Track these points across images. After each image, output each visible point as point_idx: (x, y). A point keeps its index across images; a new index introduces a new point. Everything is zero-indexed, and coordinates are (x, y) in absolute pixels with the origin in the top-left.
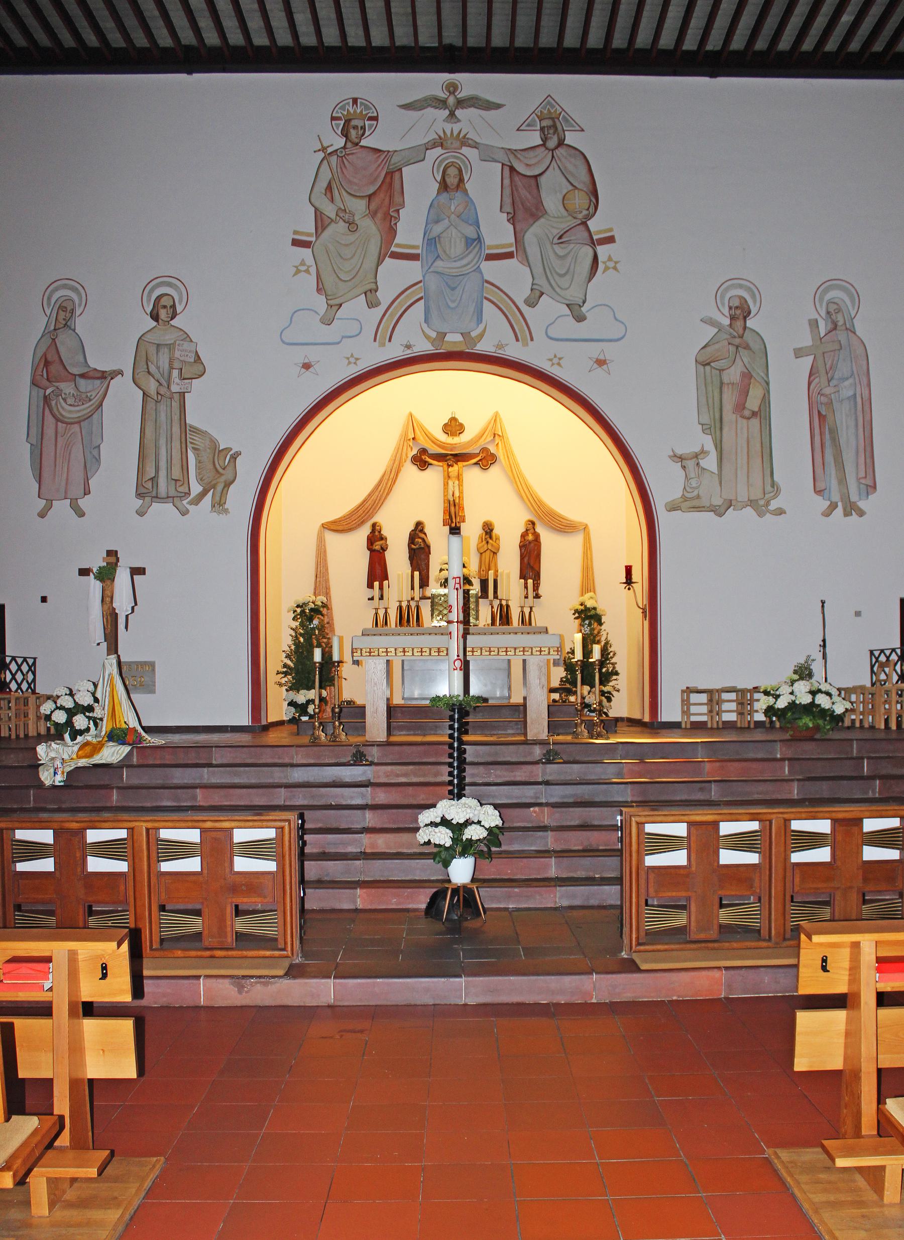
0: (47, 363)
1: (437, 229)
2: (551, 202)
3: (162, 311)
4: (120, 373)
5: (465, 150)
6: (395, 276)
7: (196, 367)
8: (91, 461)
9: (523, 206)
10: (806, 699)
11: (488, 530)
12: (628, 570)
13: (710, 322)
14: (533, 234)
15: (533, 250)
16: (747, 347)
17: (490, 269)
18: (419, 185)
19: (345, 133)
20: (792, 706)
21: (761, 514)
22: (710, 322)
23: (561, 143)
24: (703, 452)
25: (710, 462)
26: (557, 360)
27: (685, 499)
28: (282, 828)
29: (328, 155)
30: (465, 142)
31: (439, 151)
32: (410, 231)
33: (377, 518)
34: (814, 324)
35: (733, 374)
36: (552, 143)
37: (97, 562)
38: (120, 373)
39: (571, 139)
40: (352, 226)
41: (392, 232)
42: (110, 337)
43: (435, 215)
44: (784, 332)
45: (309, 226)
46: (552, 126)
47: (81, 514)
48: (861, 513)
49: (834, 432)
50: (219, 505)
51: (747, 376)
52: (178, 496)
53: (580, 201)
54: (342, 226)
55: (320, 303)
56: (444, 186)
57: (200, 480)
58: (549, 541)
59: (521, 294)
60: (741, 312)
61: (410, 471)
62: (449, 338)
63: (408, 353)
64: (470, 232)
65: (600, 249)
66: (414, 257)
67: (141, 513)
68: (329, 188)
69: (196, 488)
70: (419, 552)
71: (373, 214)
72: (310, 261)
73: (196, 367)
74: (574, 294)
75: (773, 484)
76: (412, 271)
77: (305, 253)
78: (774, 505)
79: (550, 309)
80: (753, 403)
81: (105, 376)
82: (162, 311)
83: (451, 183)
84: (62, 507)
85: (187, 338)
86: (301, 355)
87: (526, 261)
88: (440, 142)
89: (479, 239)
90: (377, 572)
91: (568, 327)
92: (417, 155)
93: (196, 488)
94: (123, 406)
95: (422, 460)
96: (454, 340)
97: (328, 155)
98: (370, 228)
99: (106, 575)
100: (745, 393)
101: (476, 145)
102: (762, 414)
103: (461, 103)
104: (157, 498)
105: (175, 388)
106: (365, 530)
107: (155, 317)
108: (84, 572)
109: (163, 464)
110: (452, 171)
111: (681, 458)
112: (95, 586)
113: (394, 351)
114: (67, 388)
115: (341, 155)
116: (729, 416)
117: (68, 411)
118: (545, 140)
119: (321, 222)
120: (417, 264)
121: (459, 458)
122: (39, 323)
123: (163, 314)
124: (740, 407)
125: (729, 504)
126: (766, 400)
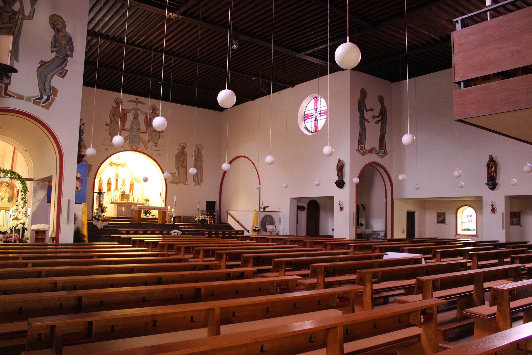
1: (133, 126)
11: (124, 181)
13: (178, 149)
17: (142, 135)
18: (130, 117)
19: (117, 104)
23: (155, 113)
25: (177, 175)
26: (152, 154)
30: (138, 110)
32: (128, 125)
34: (195, 151)
35: (181, 159)
41: (124, 125)
43: (133, 123)
44: (191, 151)
45: (109, 122)
51: (184, 160)
56: (134, 118)
59: (147, 140)
60: (183, 148)
64: (138, 127)
65: (161, 134)
66: (128, 131)
70: (109, 184)
77: (108, 127)
83: (136, 118)
88: (134, 109)
92: (130, 111)
96: (134, 147)
100: (183, 163)
101: (140, 111)
116: (180, 167)
119: (111, 121)
124: (182, 165)
125: (179, 183)
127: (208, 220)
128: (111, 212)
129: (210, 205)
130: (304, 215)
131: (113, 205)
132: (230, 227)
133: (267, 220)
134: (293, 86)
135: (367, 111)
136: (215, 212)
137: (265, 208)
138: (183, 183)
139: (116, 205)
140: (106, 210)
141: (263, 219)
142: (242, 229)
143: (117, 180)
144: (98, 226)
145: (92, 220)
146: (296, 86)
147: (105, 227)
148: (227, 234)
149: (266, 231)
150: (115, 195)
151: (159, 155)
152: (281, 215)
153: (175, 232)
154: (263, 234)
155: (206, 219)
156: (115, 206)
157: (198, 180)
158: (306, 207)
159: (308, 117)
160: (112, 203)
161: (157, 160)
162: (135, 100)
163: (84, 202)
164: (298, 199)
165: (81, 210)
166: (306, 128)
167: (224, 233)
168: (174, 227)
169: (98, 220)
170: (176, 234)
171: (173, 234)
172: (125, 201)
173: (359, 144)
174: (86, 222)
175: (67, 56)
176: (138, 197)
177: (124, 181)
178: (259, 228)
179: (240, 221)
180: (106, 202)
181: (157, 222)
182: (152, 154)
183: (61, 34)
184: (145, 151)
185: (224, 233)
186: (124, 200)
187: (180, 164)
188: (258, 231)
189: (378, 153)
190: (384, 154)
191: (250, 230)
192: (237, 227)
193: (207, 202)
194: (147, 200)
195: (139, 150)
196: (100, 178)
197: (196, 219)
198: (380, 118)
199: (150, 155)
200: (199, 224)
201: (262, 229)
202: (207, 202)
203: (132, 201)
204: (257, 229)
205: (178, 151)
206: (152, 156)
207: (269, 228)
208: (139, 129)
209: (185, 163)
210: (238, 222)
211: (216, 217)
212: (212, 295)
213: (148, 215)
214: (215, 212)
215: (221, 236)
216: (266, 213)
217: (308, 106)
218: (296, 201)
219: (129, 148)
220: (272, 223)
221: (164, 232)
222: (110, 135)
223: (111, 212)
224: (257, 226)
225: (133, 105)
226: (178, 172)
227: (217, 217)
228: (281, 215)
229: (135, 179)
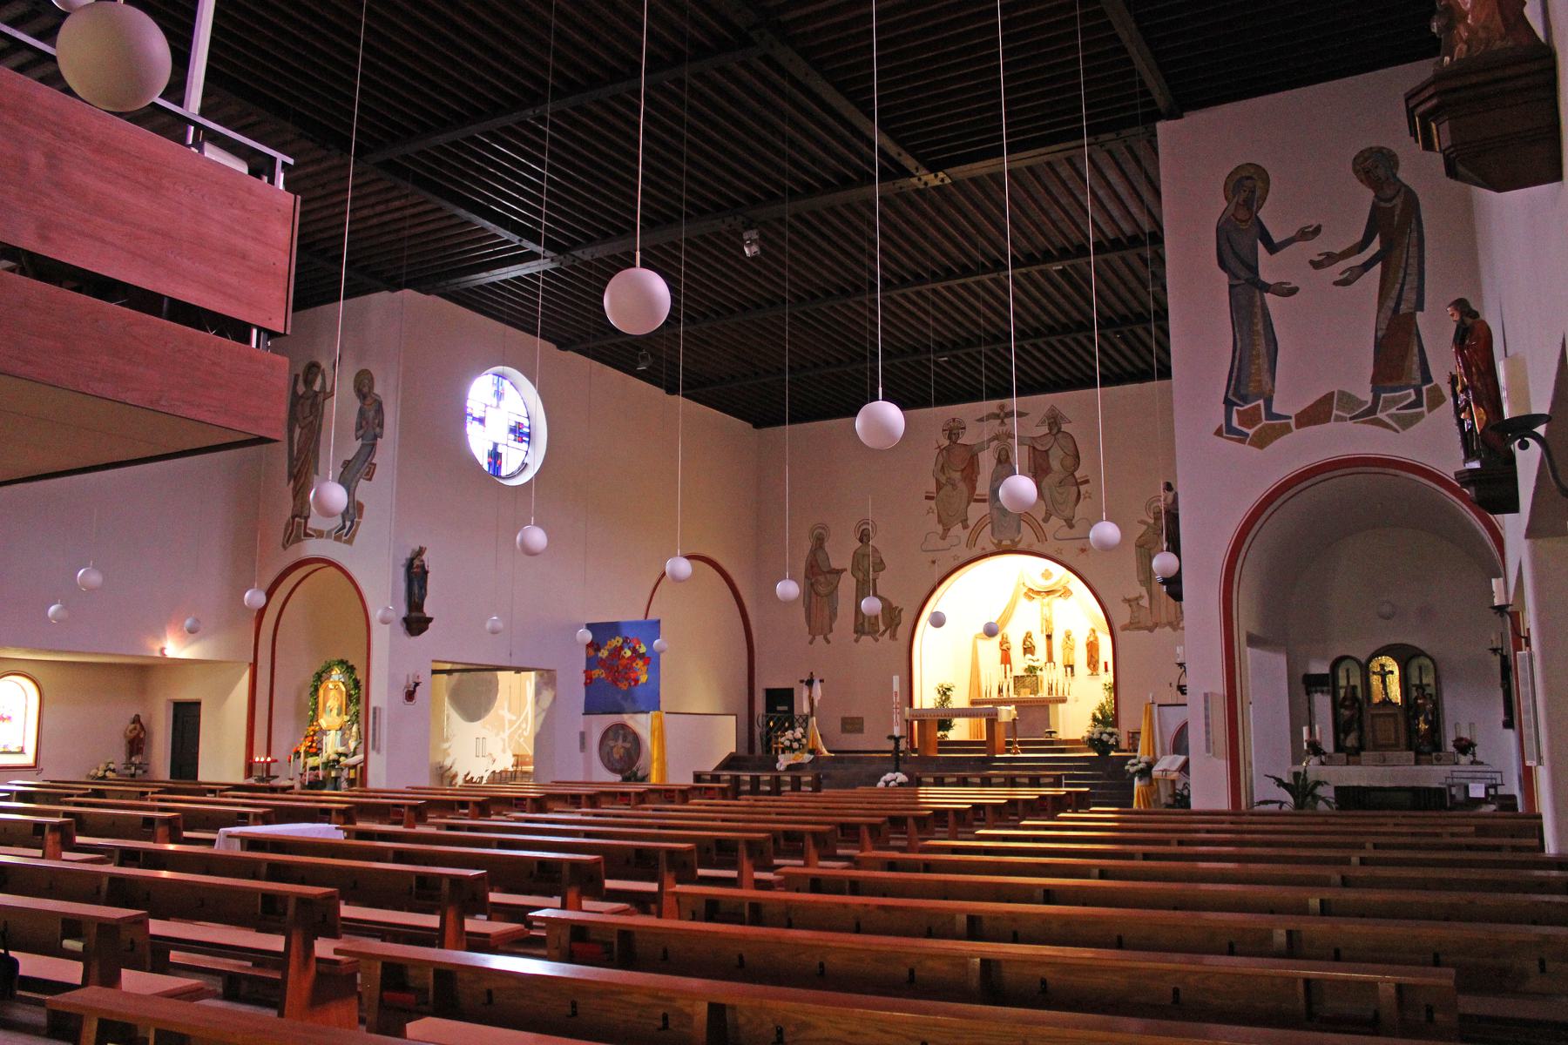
2: (1055, 464)
3: (864, 537)
6: (976, 512)
7: (880, 566)
8: (833, 615)
23: (1059, 431)
24: (1141, 597)
25: (1145, 602)
26: (1060, 551)
28: (22, 752)
39: (1064, 428)
40: (954, 486)
41: (974, 488)
42: (840, 555)
45: (932, 487)
46: (1054, 421)
47: (828, 642)
50: (893, 637)
53: (1069, 461)
54: (949, 487)
55: (940, 528)
56: (999, 461)
61: (1023, 601)
65: (1083, 488)
66: (984, 501)
67: (857, 641)
69: (882, 628)
73: (880, 566)
74: (1068, 513)
76: (984, 508)
77: (932, 503)
79: (1055, 522)
81: (839, 572)
82: (864, 537)
84: (820, 638)
86: (931, 556)
88: (996, 438)
90: (1006, 659)
91: (1065, 532)
93: (882, 628)
95: (1032, 593)
96: (1006, 542)
98: (962, 487)
99: (810, 683)
104: (864, 633)
107: (861, 540)
111: (1128, 601)
113: (977, 551)
114: (821, 579)
115: (947, 449)
117: (822, 589)
119: (939, 486)
121: (1049, 593)
122: (807, 545)
125: (1156, 625)
135: (1272, 248)
138: (1170, 624)
143: (1049, 637)
146: (570, 354)
148: (766, 783)
167: (755, 782)
172: (1026, 694)
173: (1228, 403)
175: (375, 437)
182: (1060, 551)
183: (369, 401)
184: (1037, 547)
185: (755, 782)
189: (1372, 410)
190: (1417, 403)
195: (1021, 546)
198: (1375, 246)
199: (957, 563)
205: (1144, 527)
206: (1060, 557)
212: (665, 957)
215: (747, 788)
221: (1491, 808)
222: (940, 521)
226: (1150, 592)
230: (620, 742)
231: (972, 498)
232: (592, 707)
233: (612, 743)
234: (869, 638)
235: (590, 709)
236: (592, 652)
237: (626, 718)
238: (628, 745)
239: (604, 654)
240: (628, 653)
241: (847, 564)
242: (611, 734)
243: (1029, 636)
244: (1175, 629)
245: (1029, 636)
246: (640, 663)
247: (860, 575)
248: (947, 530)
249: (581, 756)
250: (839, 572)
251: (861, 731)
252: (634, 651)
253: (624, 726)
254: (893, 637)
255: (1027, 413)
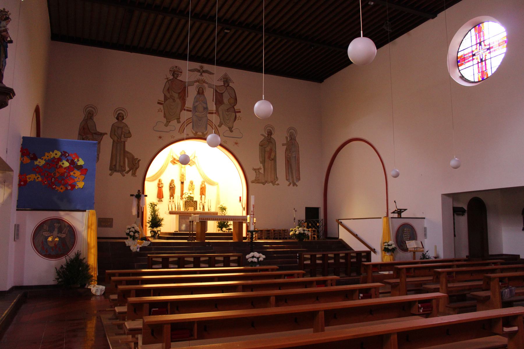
0: (84, 129)
1: (196, 104)
2: (226, 101)
3: (120, 117)
4: (106, 134)
5: (204, 84)
9: (219, 101)
10: (302, 232)
11: (192, 183)
12: (240, 197)
13: (263, 135)
14: (222, 108)
15: (220, 113)
16: (271, 142)
18: (192, 92)
19: (173, 75)
20: (300, 233)
21: (274, 185)
22: (263, 135)
23: (228, 85)
24: (260, 168)
25: (262, 171)
27: (256, 180)
29: (168, 80)
31: (197, 83)
32: (189, 103)
33: (161, 178)
34: (287, 138)
35: (268, 149)
36: (226, 85)
37: (136, 193)
38: (106, 134)
39: (231, 85)
41: (184, 103)
42: (104, 123)
43: (196, 100)
44: (280, 138)
45: (163, 99)
46: (226, 81)
48: (297, 186)
49: (291, 165)
50: (134, 174)
51: (271, 150)
52: (122, 170)
53: (232, 101)
55: (165, 121)
56: (199, 93)
57: (129, 167)
58: (208, 188)
60: (270, 133)
61: (170, 164)
62: (199, 133)
63: (188, 137)
64: (205, 105)
65: (237, 114)
66: (190, 111)
67: (111, 175)
68: (168, 89)
69: (127, 169)
70: (172, 189)
71: (180, 98)
72: (162, 108)
75: (277, 177)
76: (189, 115)
77: (161, 106)
78: (277, 183)
80: (272, 157)
81: (102, 135)
82: (120, 117)
83: (201, 92)
85: (127, 126)
87: (219, 115)
88: (198, 81)
89: (207, 108)
91: (228, 133)
92: (191, 84)
93: (127, 169)
94: (107, 143)
97: (168, 80)
98: (178, 101)
101: (207, 83)
102: (274, 160)
103: (204, 72)
104: (116, 171)
105: (122, 140)
106: (157, 182)
107: (117, 119)
108: (132, 195)
109: (118, 160)
110: (201, 89)
111: (255, 169)
112: (135, 201)
116: (267, 160)
118: (224, 84)
119: (166, 98)
120: (190, 113)
123: (120, 118)
124: (269, 157)
125: (266, 182)
126: (275, 156)
127: (310, 234)
128: (170, 225)
129: (312, 214)
130: (463, 221)
131: (174, 216)
132: (343, 245)
133: (404, 232)
134: (434, 15)
136: (318, 222)
137: (399, 212)
138: (272, 182)
139: (178, 215)
140: (162, 223)
141: (399, 229)
142: (367, 249)
143: (182, 183)
144: (132, 248)
145: (127, 238)
146: (438, 15)
147: (142, 249)
149: (406, 250)
150: (179, 203)
151: (236, 143)
152: (426, 224)
153: (253, 257)
154: (402, 256)
155: (306, 232)
156: (176, 217)
157: (293, 177)
158: (466, 208)
159: (464, 59)
160: (171, 213)
161: (235, 153)
162: (199, 68)
163: (91, 208)
164: (454, 196)
165: (85, 221)
166: (462, 77)
168: (253, 247)
169: (134, 238)
170: (255, 260)
171: (250, 260)
172: (191, 209)
174: (93, 242)
176: (210, 204)
177: (192, 183)
178: (394, 246)
179: (360, 235)
180: (163, 211)
181: (231, 239)
186: (190, 208)
187: (267, 156)
188: (393, 250)
191: (378, 249)
192: (357, 246)
193: (307, 208)
194: (223, 209)
196: (160, 181)
197: (291, 233)
200: (296, 240)
201: (397, 247)
202: (307, 208)
203: (201, 210)
204: (390, 248)
207: (411, 244)
208: (206, 108)
209: (273, 154)
210: (356, 236)
211: (321, 229)
213: (224, 229)
214: (318, 222)
216: (401, 222)
217: (466, 42)
218: (451, 200)
219: (192, 135)
220: (413, 236)
222: (165, 116)
223: (170, 225)
224: (390, 243)
225: (196, 76)
227: (321, 229)
228: (426, 224)
229: (199, 178)
230: (55, 233)
231: (183, 109)
232: (26, 202)
233: (46, 234)
234: (119, 174)
235: (22, 206)
236: (27, 160)
237: (65, 216)
238: (64, 236)
239: (40, 162)
240: (66, 164)
241: (107, 129)
242: (45, 226)
243: (172, 181)
244: (274, 184)
245: (172, 181)
246: (77, 173)
247: (116, 138)
248: (168, 122)
249: (12, 244)
250: (102, 135)
251: (111, 226)
252: (72, 163)
253: (60, 221)
254: (134, 174)
255: (217, 73)
